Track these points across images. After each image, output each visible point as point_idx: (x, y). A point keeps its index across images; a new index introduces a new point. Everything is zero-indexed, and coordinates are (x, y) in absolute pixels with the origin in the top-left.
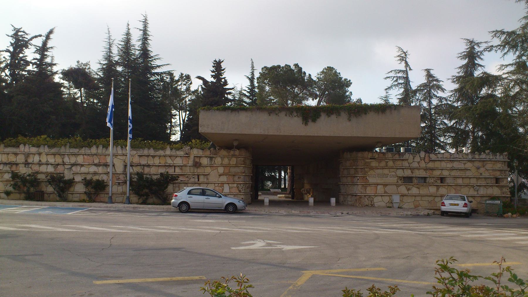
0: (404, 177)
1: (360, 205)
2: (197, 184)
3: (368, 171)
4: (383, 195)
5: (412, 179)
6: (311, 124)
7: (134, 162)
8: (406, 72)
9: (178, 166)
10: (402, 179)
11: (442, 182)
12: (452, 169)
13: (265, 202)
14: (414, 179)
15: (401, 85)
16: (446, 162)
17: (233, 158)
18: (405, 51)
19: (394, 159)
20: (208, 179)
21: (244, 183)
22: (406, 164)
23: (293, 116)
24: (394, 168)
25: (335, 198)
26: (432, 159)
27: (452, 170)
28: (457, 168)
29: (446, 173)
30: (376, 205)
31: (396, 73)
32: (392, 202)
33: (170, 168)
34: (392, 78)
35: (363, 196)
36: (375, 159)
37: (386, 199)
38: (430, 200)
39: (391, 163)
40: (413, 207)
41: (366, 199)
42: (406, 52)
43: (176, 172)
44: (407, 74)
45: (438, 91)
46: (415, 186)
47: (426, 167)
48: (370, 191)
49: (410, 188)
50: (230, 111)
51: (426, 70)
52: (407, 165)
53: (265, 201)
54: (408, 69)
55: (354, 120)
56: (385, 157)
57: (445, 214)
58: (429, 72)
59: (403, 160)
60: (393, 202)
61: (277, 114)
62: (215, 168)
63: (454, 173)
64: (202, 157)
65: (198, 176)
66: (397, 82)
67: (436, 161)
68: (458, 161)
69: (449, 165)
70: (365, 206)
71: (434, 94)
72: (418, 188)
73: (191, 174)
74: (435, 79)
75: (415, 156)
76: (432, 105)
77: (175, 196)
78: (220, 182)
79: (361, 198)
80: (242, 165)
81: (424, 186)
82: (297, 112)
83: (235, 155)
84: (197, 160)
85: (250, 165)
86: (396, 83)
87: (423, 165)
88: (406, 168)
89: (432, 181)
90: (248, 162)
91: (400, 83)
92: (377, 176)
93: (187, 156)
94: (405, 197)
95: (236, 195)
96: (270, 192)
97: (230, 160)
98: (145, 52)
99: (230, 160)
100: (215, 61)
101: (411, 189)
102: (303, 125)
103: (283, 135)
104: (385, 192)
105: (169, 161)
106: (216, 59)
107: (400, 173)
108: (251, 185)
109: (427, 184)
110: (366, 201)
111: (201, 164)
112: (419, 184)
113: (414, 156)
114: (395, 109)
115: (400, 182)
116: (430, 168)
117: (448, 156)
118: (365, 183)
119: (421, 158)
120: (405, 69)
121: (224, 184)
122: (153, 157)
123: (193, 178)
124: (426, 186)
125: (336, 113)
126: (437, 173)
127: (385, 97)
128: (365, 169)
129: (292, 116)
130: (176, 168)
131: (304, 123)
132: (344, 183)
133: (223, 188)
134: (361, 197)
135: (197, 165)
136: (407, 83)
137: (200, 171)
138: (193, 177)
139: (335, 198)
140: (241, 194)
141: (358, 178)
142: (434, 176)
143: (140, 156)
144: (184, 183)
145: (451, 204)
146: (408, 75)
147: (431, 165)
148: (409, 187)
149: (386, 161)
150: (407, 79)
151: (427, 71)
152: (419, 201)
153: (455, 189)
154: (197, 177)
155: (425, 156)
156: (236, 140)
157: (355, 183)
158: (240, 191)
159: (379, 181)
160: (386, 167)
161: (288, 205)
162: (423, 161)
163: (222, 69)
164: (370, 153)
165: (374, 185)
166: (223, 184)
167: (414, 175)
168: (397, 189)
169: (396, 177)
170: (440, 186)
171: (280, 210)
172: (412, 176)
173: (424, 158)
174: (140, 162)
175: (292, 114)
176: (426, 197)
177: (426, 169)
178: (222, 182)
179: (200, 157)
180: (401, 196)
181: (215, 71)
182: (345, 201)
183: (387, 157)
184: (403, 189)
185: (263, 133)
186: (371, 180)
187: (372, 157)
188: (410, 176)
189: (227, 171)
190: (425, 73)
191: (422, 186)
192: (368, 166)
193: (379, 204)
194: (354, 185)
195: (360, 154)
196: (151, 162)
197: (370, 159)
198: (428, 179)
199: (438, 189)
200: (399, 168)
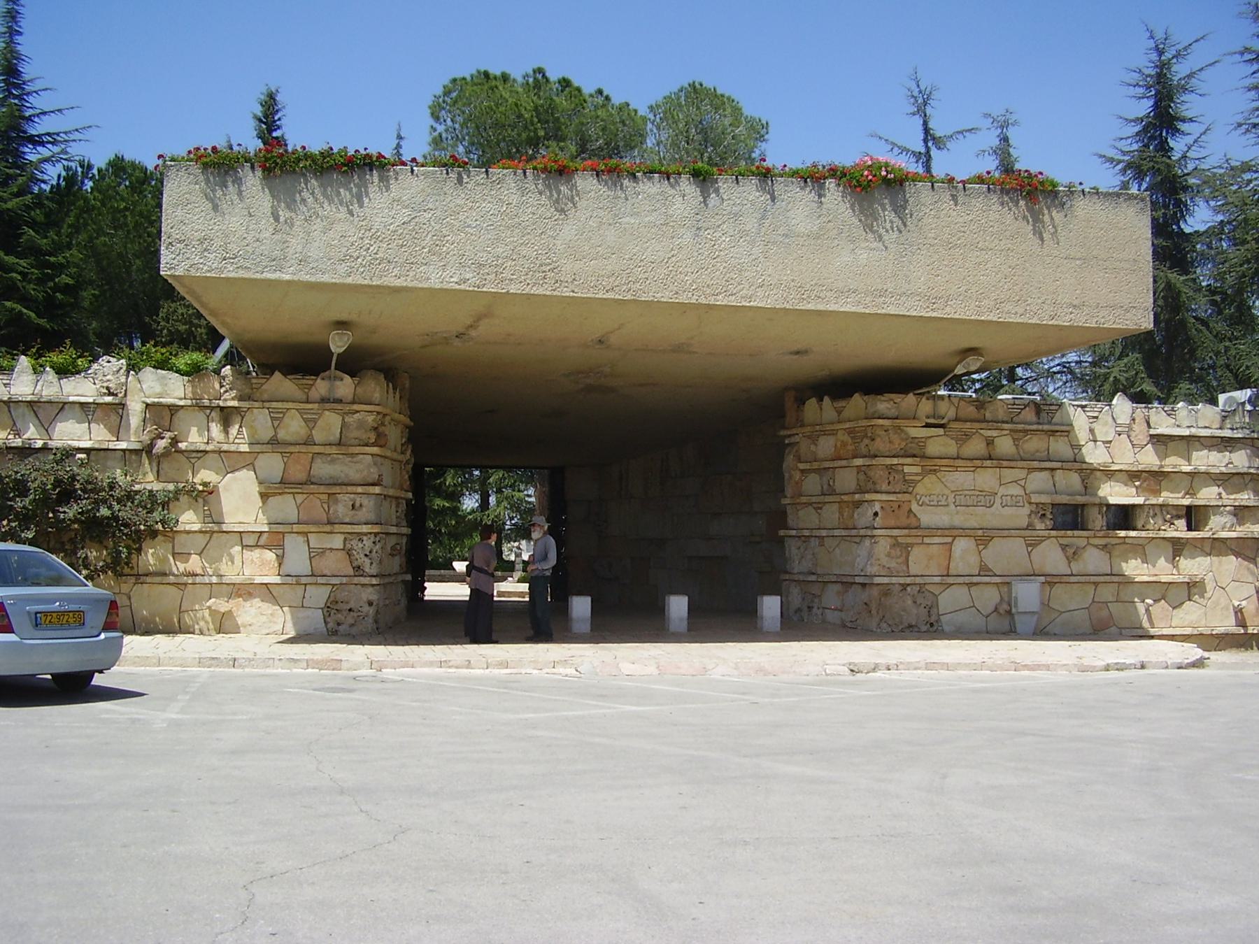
1: (884, 625)
4: (975, 579)
19: (1020, 431)
20: (220, 527)
21: (376, 529)
25: (589, 599)
29: (1208, 494)
39: (1005, 445)
48: (922, 561)
60: (1014, 610)
70: (902, 631)
77: (1245, 626)
80: (367, 445)
85: (402, 453)
90: (395, 435)
92: (951, 499)
96: (451, 572)
104: (984, 570)
108: (404, 540)
128: (906, 469)
132: (806, 533)
134: (886, 591)
139: (589, 599)
140: (366, 580)
141: (877, 507)
149: (986, 438)
152: (1109, 604)
156: (342, 325)
157: (862, 532)
158: (359, 567)
160: (991, 458)
162: (1124, 436)
168: (1029, 553)
169: (1027, 505)
182: (810, 608)
184: (1051, 556)
185: (470, 280)
194: (857, 540)
195: (883, 404)
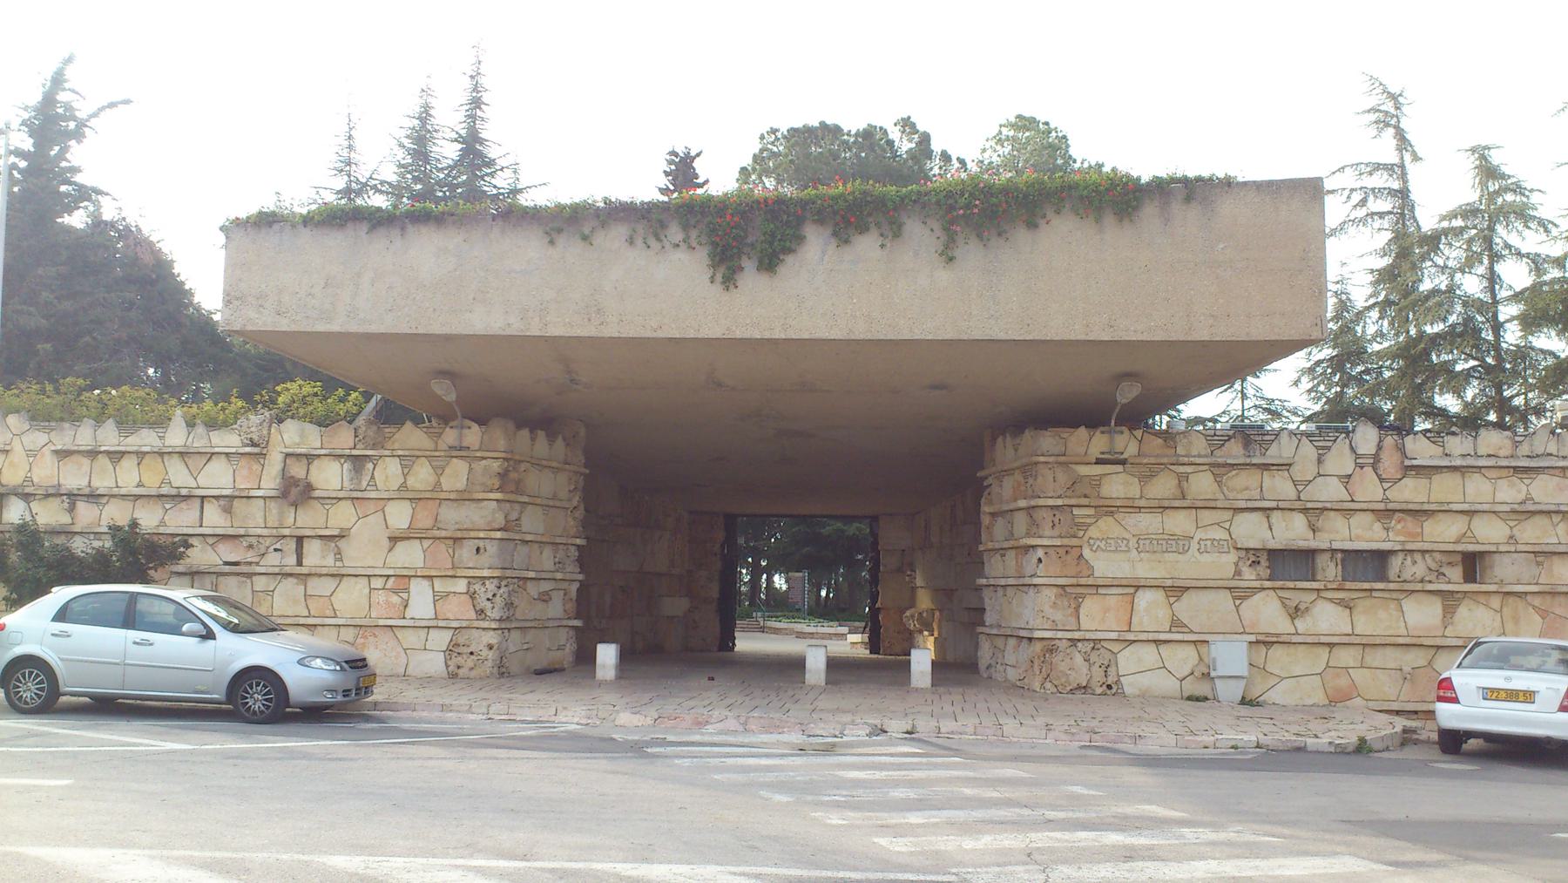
0: (1273, 554)
1: (1048, 685)
2: (295, 581)
3: (1088, 521)
4: (1163, 637)
5: (1313, 560)
6: (751, 279)
7: (36, 480)
8: (1399, 170)
9: (213, 497)
10: (1264, 563)
11: (1470, 577)
12: (1524, 513)
13: (806, 671)
14: (1322, 561)
15: (1380, 221)
16: (1493, 474)
17: (454, 460)
18: (1394, 89)
20: (339, 555)
22: (1280, 487)
23: (667, 245)
24: (1219, 504)
26: (1415, 462)
27: (1523, 517)
28: (1553, 508)
29: (1489, 533)
30: (1130, 685)
31: (1360, 174)
32: (1209, 673)
33: (183, 505)
34: (1346, 193)
35: (1065, 644)
36: (1123, 462)
37: (1183, 659)
38: (1407, 669)
40: (1319, 697)
41: (1079, 659)
42: (1400, 95)
43: (204, 525)
44: (1403, 177)
45: (1527, 232)
46: (1330, 595)
47: (1386, 500)
48: (1097, 616)
49: (1302, 607)
50: (365, 227)
51: (1473, 150)
52: (1291, 492)
53: (810, 664)
54: (1407, 157)
55: (971, 254)
56: (1176, 454)
57: (1453, 742)
58: (1486, 160)
59: (1265, 467)
60: (1213, 674)
61: (585, 238)
62: (371, 507)
63: (1533, 533)
64: (319, 456)
65: (300, 540)
66: (1364, 208)
67: (1437, 469)
68: (1552, 471)
69: (1509, 492)
71: (1508, 246)
72: (1348, 606)
73: (265, 532)
74: (1509, 181)
75: (1329, 448)
76: (1501, 287)
78: (391, 572)
79: (1051, 651)
81: (1375, 594)
82: (686, 227)
83: (461, 449)
84: (297, 470)
86: (1361, 213)
87: (1369, 489)
88: (1281, 505)
89: (1418, 569)
91: (1376, 214)
92: (1133, 542)
93: (257, 451)
94: (1277, 652)
95: (463, 630)
97: (439, 471)
98: (472, 145)
99: (439, 471)
100: (674, 153)
101: (1307, 609)
102: (717, 288)
103: (617, 335)
104: (1176, 624)
105: (179, 476)
106: (673, 147)
107: (1251, 531)
109: (1392, 586)
110: (1076, 668)
111: (309, 487)
112: (1348, 585)
113: (1323, 448)
114: (1188, 199)
115: (1248, 573)
116: (1404, 506)
117: (1500, 448)
118: (1074, 581)
119: (1358, 456)
120: (1396, 160)
121: (412, 580)
122: (116, 456)
123: (276, 550)
124: (1386, 595)
125: (878, 225)
126: (1445, 532)
127: (1338, 282)
128: (1076, 511)
129: (663, 247)
130: (206, 506)
131: (719, 277)
133: (405, 596)
134: (1051, 648)
135: (296, 492)
136: (1403, 214)
137: (308, 519)
138: (278, 546)
140: (485, 624)
142: (1426, 546)
143: (63, 454)
144: (238, 574)
145: (1491, 694)
146: (1407, 182)
147: (1410, 491)
148: (1295, 598)
150: (1403, 194)
151: (1477, 155)
152: (1350, 670)
153: (1544, 614)
154: (292, 545)
155: (1379, 448)
159: (1145, 569)
160: (1182, 502)
161: (712, 679)
162: (1369, 470)
163: (700, 181)
164: (1098, 433)
165: (1120, 590)
166: (403, 580)
167: (1320, 542)
170: (1459, 595)
171: (565, 708)
172: (1313, 544)
173: (1376, 458)
174: (62, 481)
175: (663, 238)
176: (1389, 650)
177: (1385, 513)
178: (399, 572)
179: (310, 458)
180: (1258, 642)
181: (672, 188)
183: (1183, 453)
184: (1267, 612)
185: (516, 326)
186: (1105, 565)
187: (1109, 453)
188: (1303, 544)
189: (425, 521)
190: (1471, 161)
191: (1368, 594)
192: (1085, 496)
193: (1145, 681)
195: (1048, 441)
196: (102, 483)
197: (1099, 462)
198: (1395, 563)
199: (1449, 611)
200: (1242, 504)
